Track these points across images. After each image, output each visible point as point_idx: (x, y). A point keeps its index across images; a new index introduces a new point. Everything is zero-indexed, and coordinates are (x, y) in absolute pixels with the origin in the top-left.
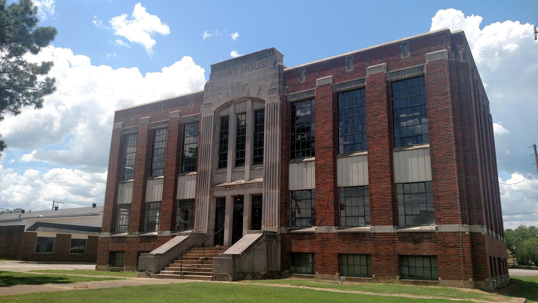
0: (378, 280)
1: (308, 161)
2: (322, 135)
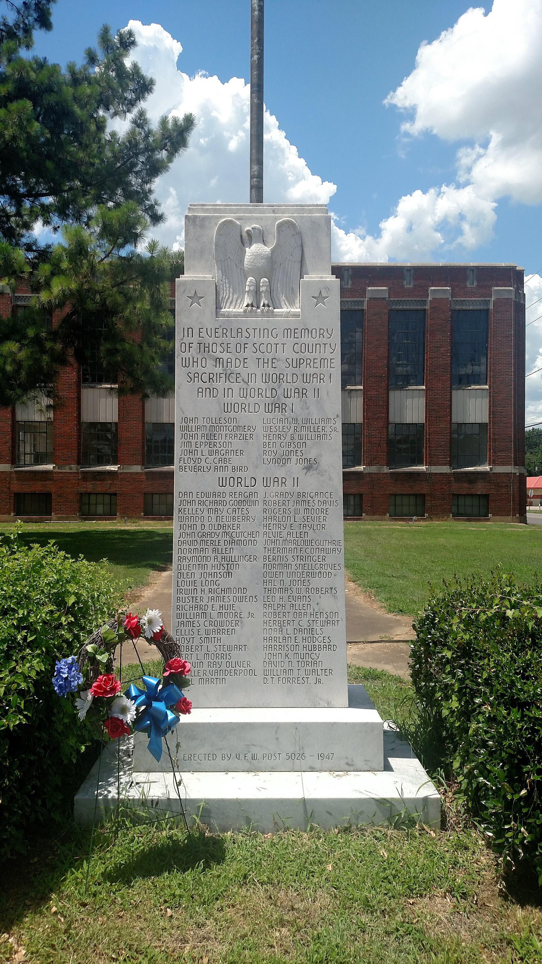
0: (431, 519)
1: (352, 390)
2: (373, 361)
